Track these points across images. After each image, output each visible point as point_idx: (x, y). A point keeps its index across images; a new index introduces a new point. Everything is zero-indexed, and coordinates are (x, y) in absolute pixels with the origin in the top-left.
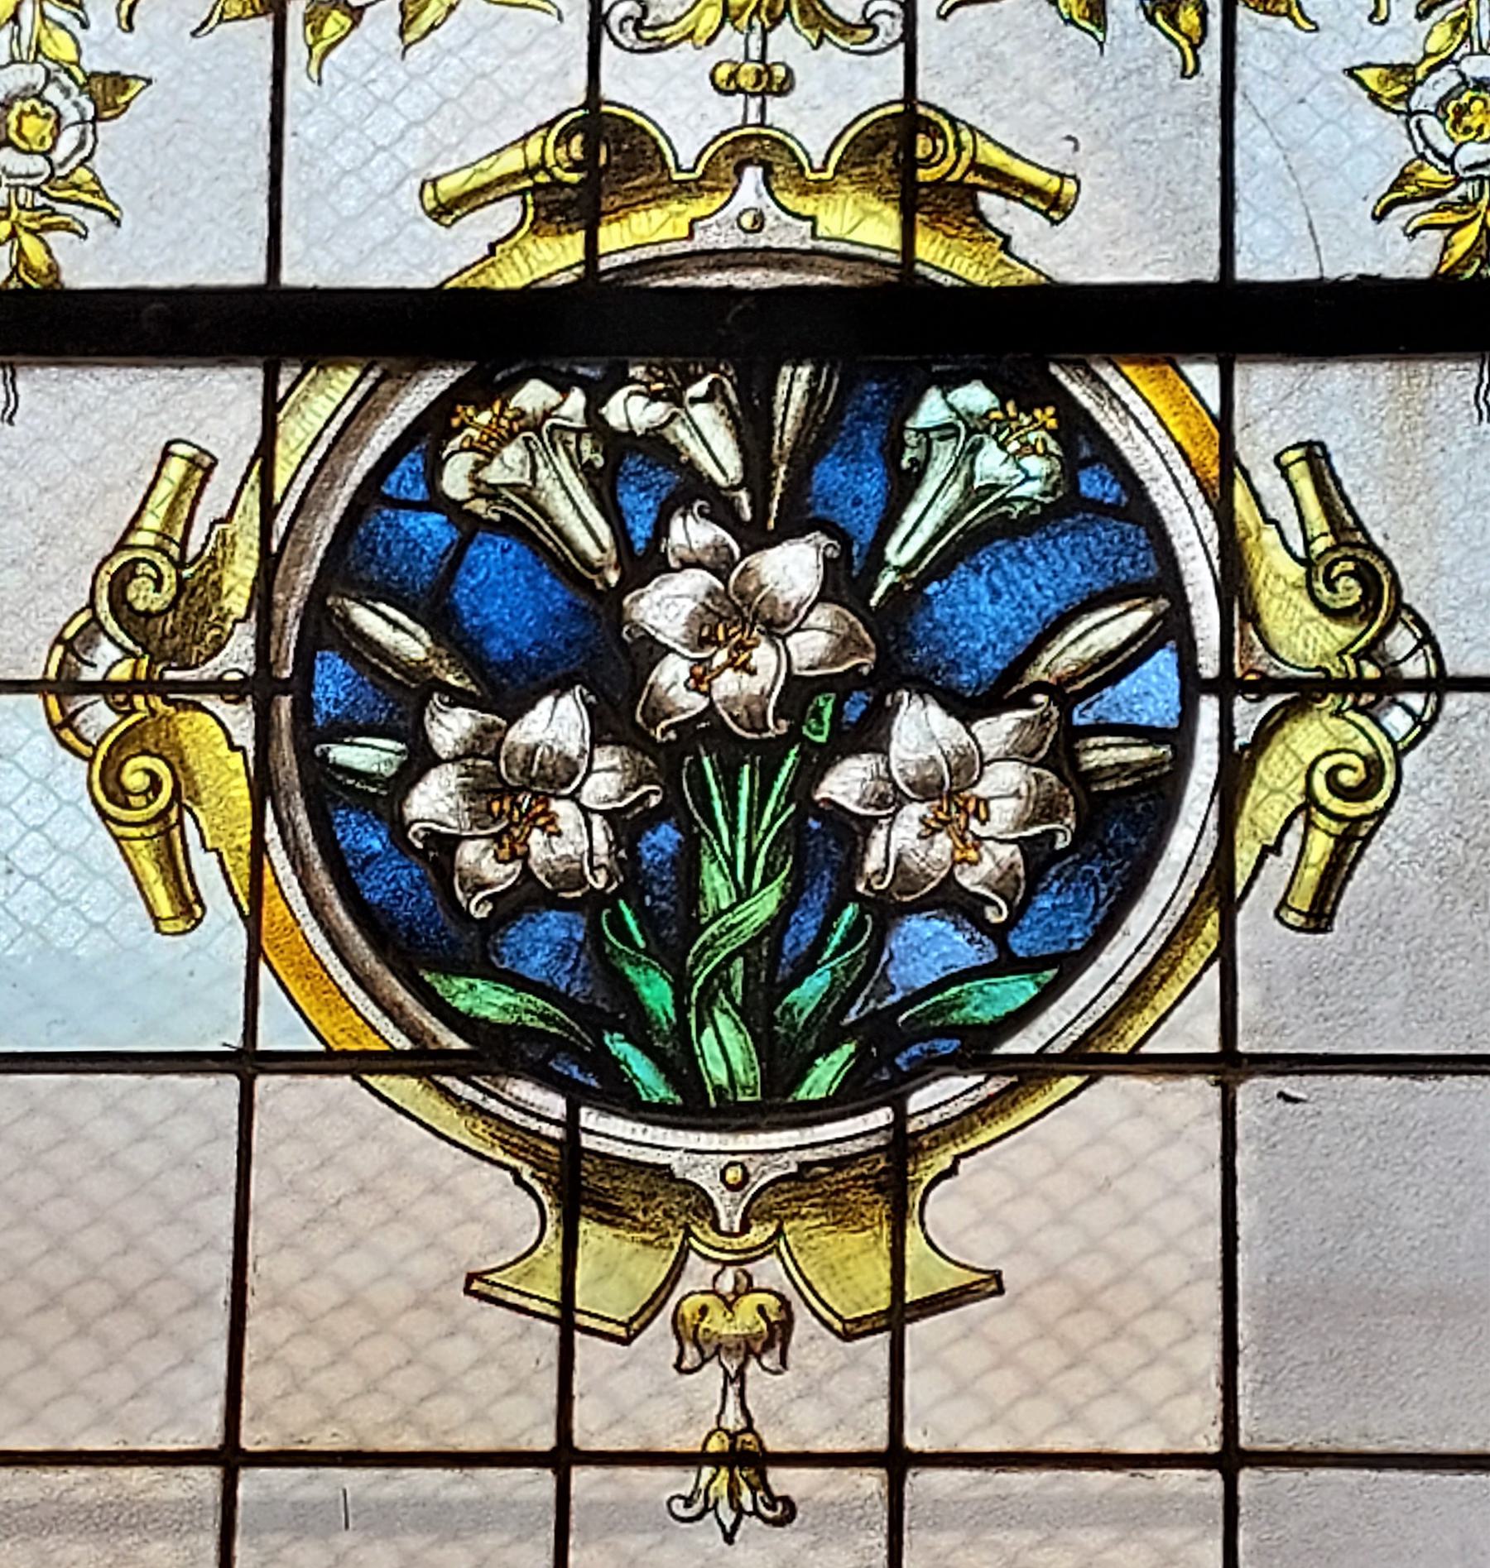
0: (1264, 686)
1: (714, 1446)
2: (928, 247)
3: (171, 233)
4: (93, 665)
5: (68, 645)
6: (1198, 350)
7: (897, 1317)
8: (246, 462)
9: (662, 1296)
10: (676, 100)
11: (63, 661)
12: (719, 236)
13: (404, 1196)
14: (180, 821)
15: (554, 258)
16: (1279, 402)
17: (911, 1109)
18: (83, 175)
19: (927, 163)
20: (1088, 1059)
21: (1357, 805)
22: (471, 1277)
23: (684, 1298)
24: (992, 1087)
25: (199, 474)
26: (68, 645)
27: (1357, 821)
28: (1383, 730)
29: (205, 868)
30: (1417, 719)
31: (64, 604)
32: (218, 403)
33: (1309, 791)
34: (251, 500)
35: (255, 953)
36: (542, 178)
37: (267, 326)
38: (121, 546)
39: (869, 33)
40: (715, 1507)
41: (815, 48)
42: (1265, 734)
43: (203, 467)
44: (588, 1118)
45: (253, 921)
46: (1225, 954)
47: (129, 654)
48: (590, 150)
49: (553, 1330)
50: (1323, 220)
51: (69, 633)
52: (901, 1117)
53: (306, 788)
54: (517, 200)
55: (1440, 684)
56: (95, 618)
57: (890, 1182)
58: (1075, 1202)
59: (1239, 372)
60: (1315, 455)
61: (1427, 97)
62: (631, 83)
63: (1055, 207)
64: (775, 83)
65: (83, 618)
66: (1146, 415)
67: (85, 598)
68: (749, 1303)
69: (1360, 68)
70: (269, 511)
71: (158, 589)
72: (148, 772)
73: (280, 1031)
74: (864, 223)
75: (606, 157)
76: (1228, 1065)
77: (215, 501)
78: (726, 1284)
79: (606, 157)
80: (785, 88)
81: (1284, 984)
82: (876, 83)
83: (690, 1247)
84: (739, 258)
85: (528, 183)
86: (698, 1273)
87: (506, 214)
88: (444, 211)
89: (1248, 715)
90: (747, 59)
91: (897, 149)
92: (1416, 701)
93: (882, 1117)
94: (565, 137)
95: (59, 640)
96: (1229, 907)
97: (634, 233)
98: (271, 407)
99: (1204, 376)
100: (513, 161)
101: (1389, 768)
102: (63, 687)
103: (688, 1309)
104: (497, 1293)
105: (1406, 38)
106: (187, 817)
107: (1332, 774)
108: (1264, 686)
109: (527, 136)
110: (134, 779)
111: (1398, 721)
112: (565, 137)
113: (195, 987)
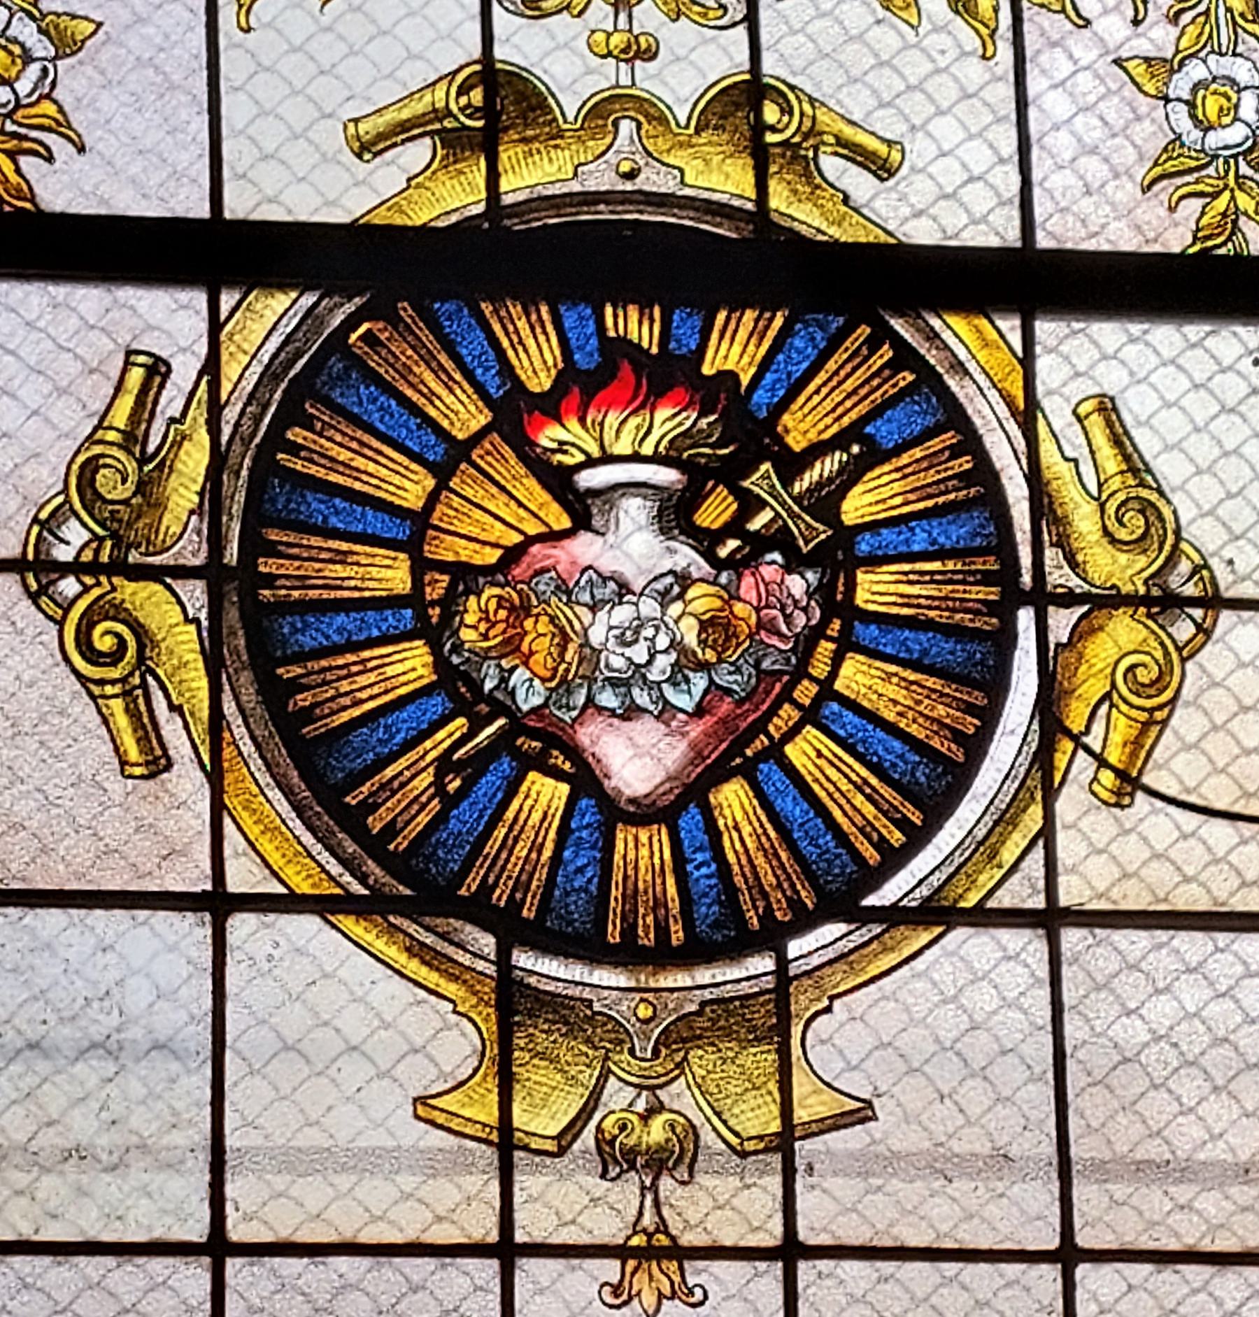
0: (1068, 599)
1: (635, 1241)
2: (779, 199)
3: (121, 166)
4: (68, 543)
5: (43, 524)
6: (1007, 307)
7: (784, 1142)
8: (194, 377)
9: (579, 1124)
10: (560, 58)
11: (39, 535)
12: (600, 179)
13: (357, 1030)
14: (144, 685)
15: (457, 196)
16: (1082, 356)
17: (791, 956)
18: (48, 108)
19: (773, 129)
20: (937, 913)
21: (1154, 698)
22: (420, 1100)
23: (605, 1117)
24: (856, 939)
25: (158, 380)
26: (43, 524)
27: (1151, 711)
28: (1169, 635)
29: (172, 729)
30: (1199, 627)
31: (47, 478)
32: (169, 318)
33: (1114, 685)
34: (198, 414)
35: (218, 808)
36: (449, 124)
37: (211, 252)
38: (90, 439)
39: (720, 12)
40: (639, 1294)
41: (674, 21)
42: (1080, 633)
43: (158, 370)
44: (523, 959)
45: (215, 777)
46: (1047, 834)
47: (96, 537)
48: (489, 97)
49: (491, 1154)
50: (1104, 206)
51: (44, 515)
52: (783, 963)
53: (262, 636)
54: (427, 141)
55: (1214, 601)
56: (67, 501)
57: (771, 1021)
58: (923, 1028)
59: (1013, 237)
60: (1107, 407)
61: (1181, 86)
62: (519, 42)
63: (882, 169)
64: (640, 52)
65: (61, 499)
66: (971, 345)
67: (60, 486)
68: (658, 1122)
69: (1127, 60)
70: (215, 409)
71: (124, 481)
72: (118, 635)
73: (243, 877)
74: (730, 180)
75: (501, 105)
76: (1051, 919)
77: (171, 401)
78: (641, 1106)
79: (501, 105)
80: (649, 55)
81: (1100, 851)
82: (725, 57)
83: (610, 1071)
84: (584, 1116)
85: (437, 126)
86: (617, 1096)
87: (418, 153)
88: (365, 149)
89: (1062, 622)
90: (616, 30)
91: (742, 104)
92: (1198, 613)
93: (763, 963)
94: (463, 90)
95: (35, 520)
96: (1050, 794)
97: (529, 174)
98: (215, 326)
99: (1010, 326)
100: (418, 107)
101: (1177, 671)
102: (35, 569)
103: (608, 1124)
104: (441, 1118)
105: (1160, 38)
106: (150, 679)
107: (1132, 668)
108: (1068, 599)
109: (434, 83)
110: (104, 644)
111: (1184, 630)
112: (463, 90)
113: (167, 831)
